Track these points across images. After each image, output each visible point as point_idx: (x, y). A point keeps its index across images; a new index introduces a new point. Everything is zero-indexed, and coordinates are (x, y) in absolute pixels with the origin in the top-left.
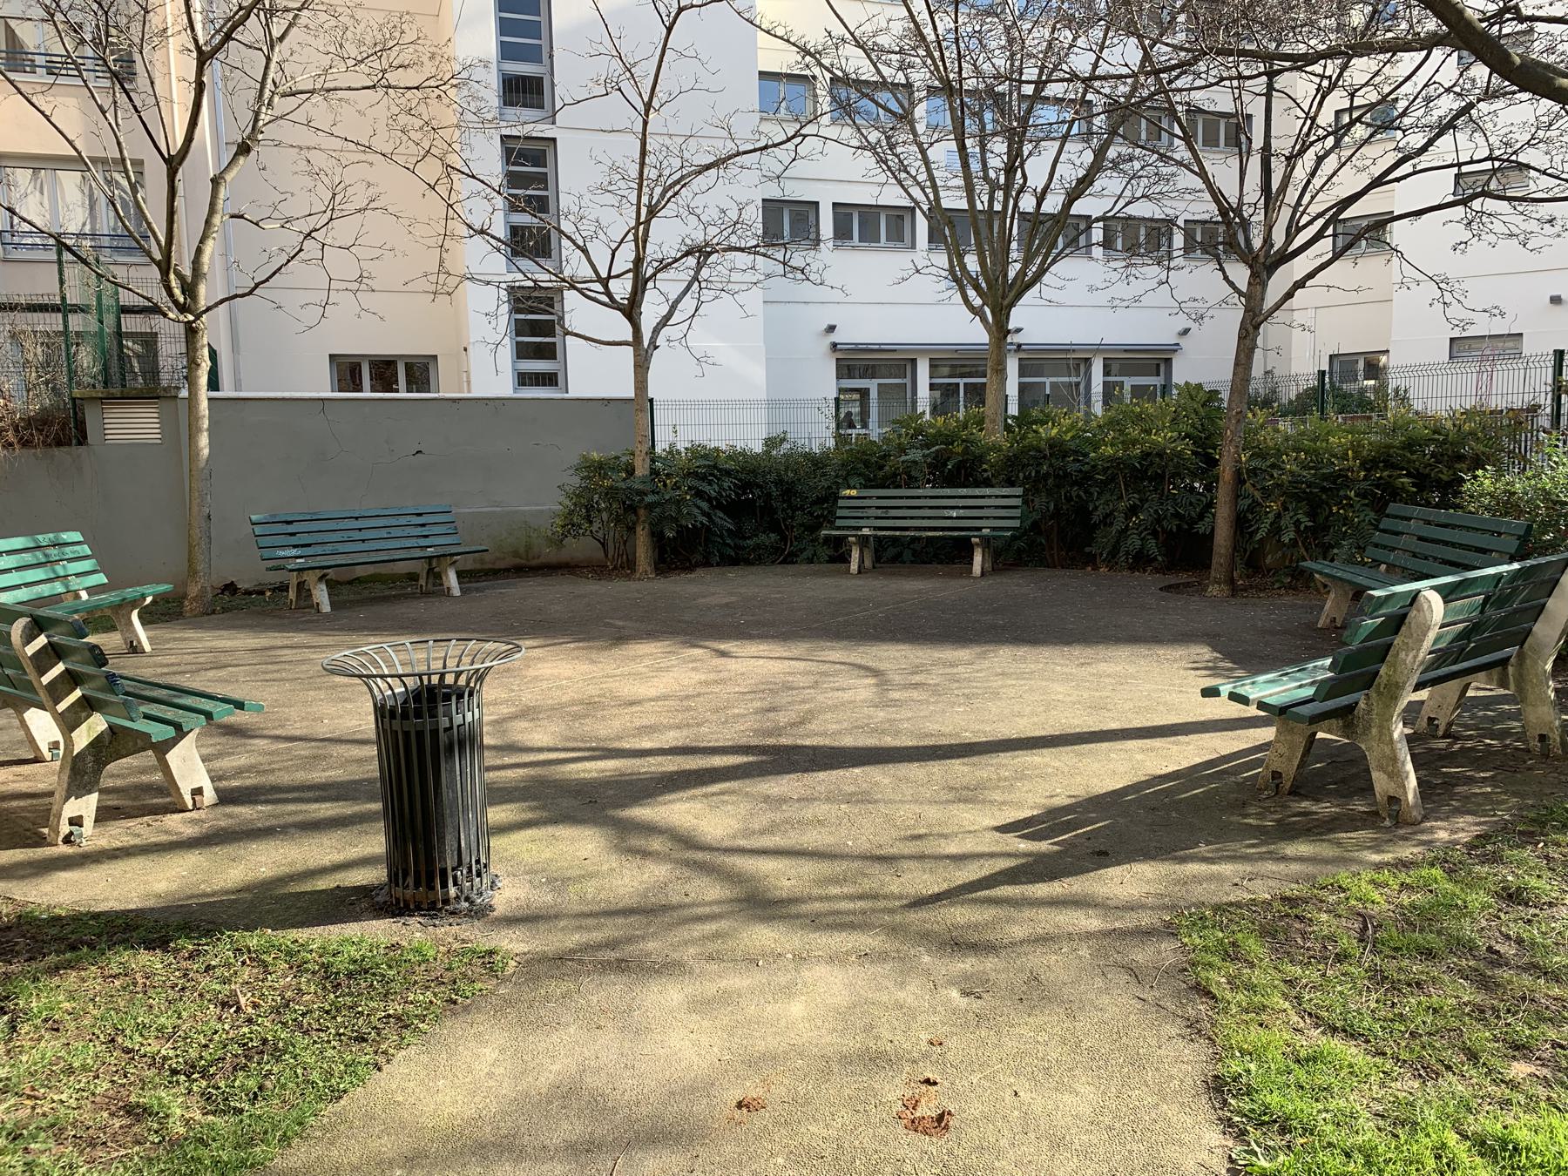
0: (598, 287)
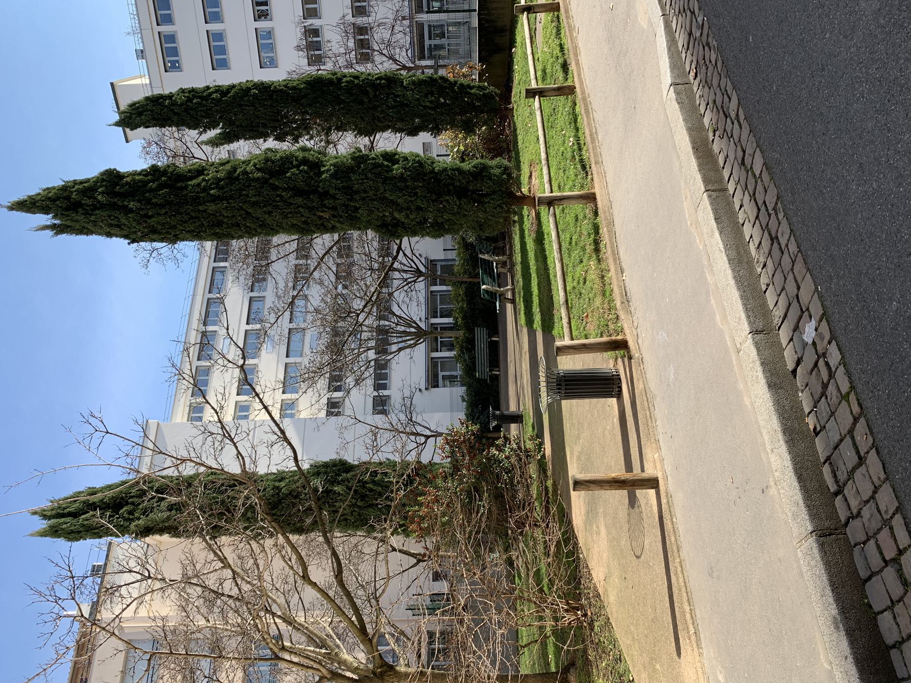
0: (420, 448)
